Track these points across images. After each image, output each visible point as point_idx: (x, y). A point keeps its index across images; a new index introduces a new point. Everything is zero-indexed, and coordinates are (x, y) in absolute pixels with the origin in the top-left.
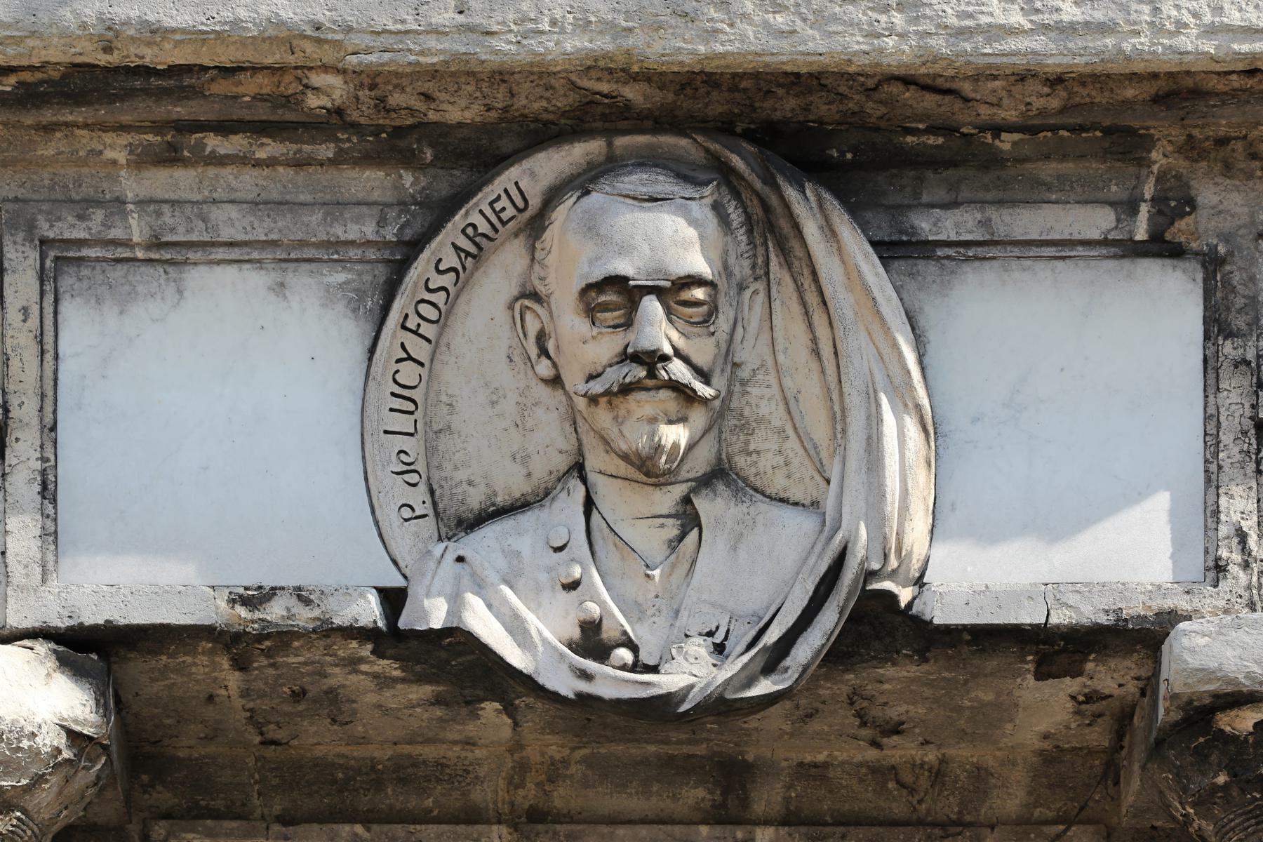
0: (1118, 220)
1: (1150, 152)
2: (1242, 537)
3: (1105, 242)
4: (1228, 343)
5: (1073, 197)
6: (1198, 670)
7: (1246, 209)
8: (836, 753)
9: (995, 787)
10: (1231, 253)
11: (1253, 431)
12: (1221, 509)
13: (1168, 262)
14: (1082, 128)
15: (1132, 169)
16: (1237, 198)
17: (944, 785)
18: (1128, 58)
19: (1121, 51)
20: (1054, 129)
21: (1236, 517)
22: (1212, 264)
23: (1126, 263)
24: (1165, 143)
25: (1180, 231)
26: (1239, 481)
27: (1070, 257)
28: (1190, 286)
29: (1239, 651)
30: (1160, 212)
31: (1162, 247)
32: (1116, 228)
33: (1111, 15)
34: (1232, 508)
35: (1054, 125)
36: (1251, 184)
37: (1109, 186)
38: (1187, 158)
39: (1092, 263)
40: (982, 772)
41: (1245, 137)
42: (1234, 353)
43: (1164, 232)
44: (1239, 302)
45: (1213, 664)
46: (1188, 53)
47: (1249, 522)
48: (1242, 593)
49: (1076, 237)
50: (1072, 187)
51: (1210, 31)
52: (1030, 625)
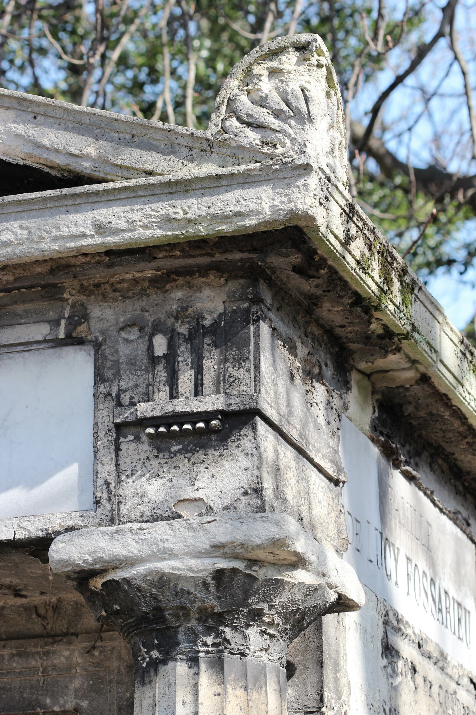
0: (51, 330)
1: (63, 294)
2: (108, 484)
3: (45, 341)
4: (102, 386)
5: (32, 320)
6: (59, 561)
7: (114, 317)
8: (8, 601)
9: (85, 613)
10: (105, 340)
11: (114, 429)
12: (99, 471)
13: (77, 347)
14: (32, 287)
15: (60, 303)
16: (109, 311)
17: (60, 613)
18: (19, 257)
19: (15, 254)
20: (18, 289)
21: (105, 475)
22: (97, 346)
23: (57, 350)
24: (70, 289)
25: (81, 330)
26: (107, 456)
27: (31, 350)
28: (88, 358)
29: (79, 549)
30: (70, 323)
31: (73, 340)
32: (50, 333)
33: (9, 237)
34: (103, 470)
35: (19, 286)
36: (116, 304)
37: (49, 313)
38: (84, 295)
39: (42, 351)
40: (79, 605)
41: (108, 282)
42: (104, 390)
43: (72, 333)
44: (109, 364)
45: (66, 557)
46: (46, 251)
47: (111, 477)
48: (108, 514)
49: (31, 340)
50: (31, 315)
51: (56, 239)
52: (6, 540)
